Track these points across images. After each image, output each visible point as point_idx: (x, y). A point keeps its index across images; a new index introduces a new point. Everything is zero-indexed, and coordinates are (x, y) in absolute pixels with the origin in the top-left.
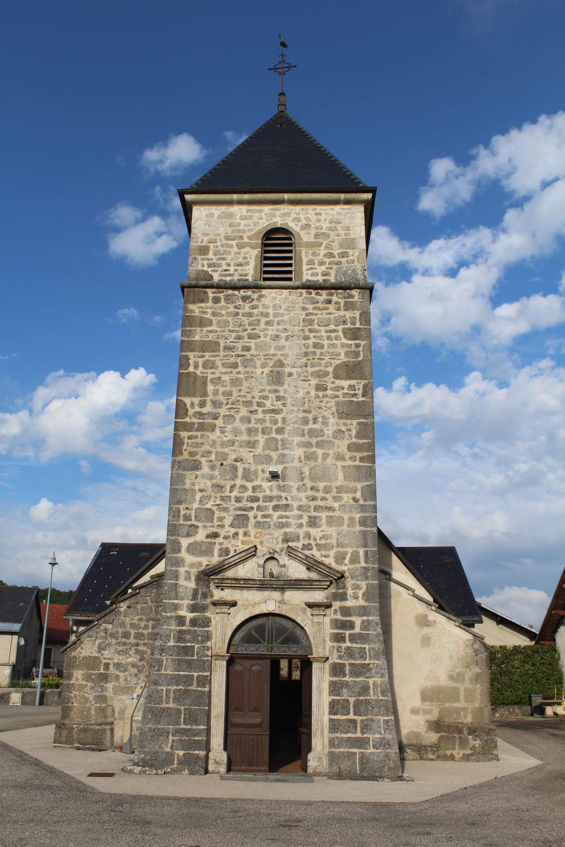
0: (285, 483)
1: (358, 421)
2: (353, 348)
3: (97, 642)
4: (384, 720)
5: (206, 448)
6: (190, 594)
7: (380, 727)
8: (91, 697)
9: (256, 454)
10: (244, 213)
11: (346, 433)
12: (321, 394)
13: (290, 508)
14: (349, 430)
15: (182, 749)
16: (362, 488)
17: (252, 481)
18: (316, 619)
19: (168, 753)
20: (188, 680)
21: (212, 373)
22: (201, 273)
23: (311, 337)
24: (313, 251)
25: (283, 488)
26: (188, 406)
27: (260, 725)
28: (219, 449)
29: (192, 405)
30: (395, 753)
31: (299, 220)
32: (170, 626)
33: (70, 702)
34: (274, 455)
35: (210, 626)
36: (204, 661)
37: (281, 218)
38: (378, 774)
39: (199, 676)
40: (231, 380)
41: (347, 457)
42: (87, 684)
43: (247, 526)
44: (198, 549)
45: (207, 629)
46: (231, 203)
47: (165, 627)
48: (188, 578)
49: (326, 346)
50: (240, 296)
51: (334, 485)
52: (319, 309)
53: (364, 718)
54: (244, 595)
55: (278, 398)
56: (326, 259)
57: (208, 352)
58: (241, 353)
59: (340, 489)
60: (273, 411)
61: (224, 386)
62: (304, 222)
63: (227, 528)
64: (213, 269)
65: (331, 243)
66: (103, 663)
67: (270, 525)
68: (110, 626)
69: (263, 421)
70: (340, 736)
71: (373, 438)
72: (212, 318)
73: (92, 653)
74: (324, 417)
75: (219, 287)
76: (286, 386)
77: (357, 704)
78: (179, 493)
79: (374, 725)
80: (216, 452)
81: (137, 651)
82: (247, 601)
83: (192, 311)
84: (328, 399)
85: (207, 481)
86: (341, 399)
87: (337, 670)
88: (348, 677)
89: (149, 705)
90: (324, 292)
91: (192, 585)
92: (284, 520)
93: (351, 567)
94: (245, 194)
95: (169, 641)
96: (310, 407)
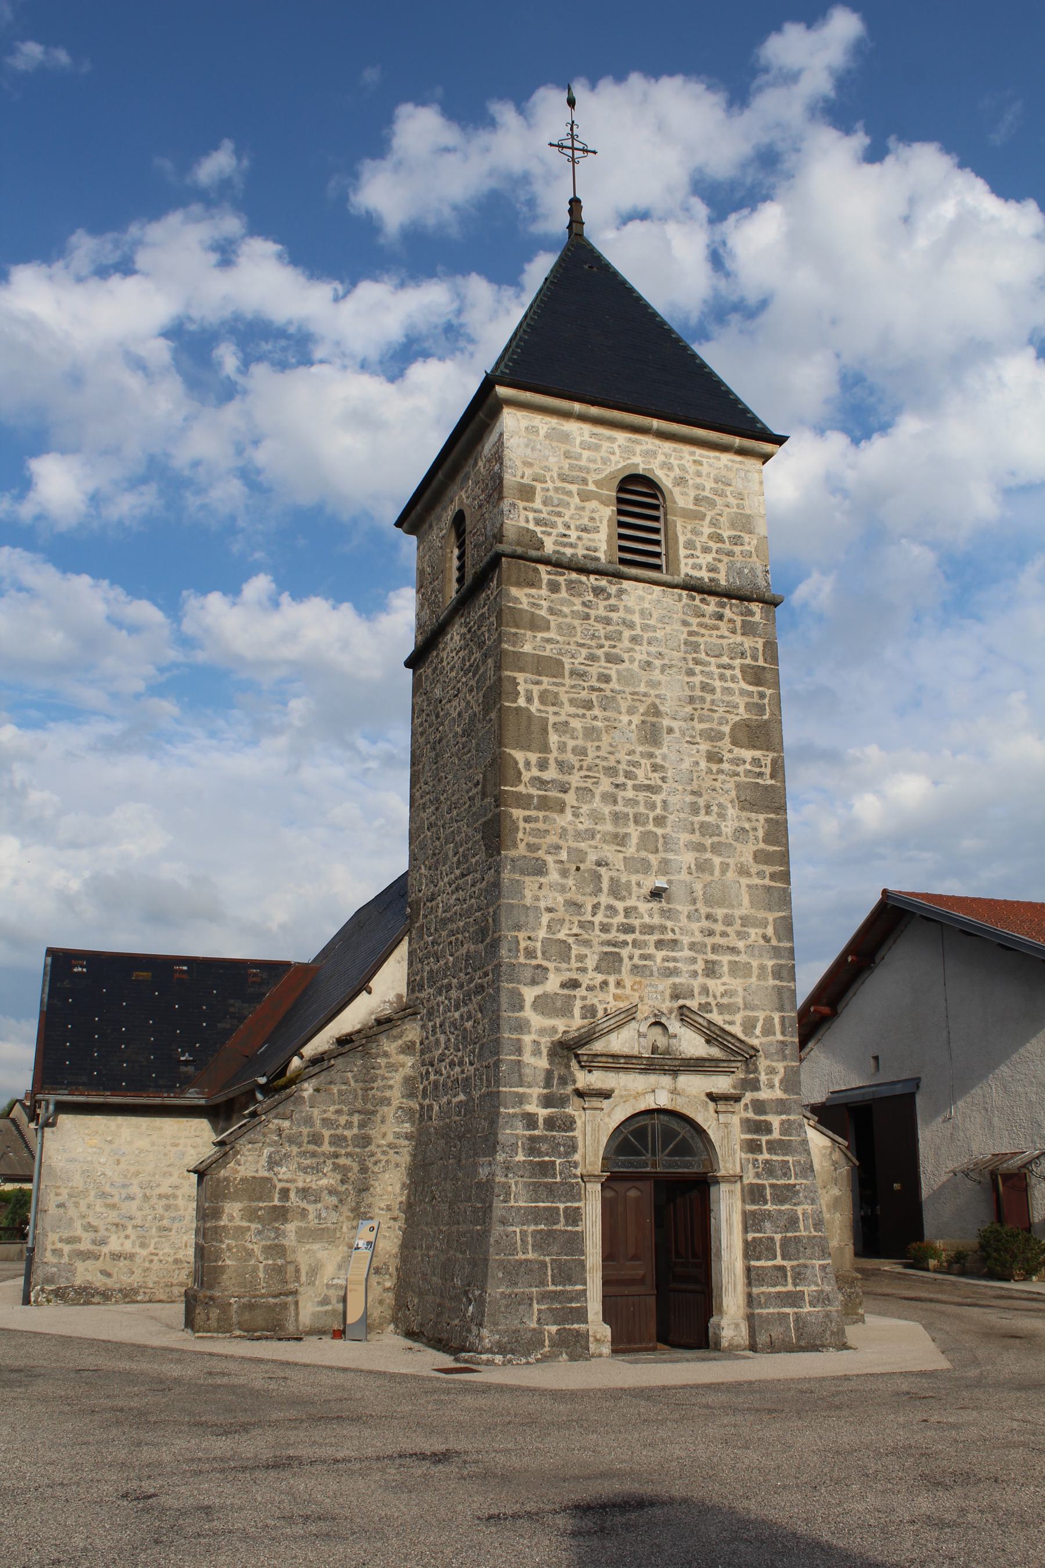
0: (671, 906)
2: (756, 700)
3: (266, 1152)
4: (820, 1265)
5: (552, 839)
6: (541, 1077)
7: (816, 1276)
8: (257, 1249)
9: (627, 855)
10: (586, 438)
11: (751, 833)
12: (714, 767)
13: (679, 945)
14: (755, 829)
15: (555, 1323)
16: (775, 920)
17: (622, 899)
19: (534, 1330)
21: (555, 713)
22: (525, 532)
23: (697, 671)
24: (693, 526)
25: (668, 914)
26: (521, 766)
27: (642, 1281)
28: (572, 844)
29: (528, 764)
30: (837, 1311)
31: (670, 468)
33: (221, 1258)
36: (572, 1185)
37: (643, 459)
38: (818, 1342)
39: (566, 1208)
40: (585, 728)
42: (249, 1227)
43: (620, 972)
45: (571, 1134)
46: (567, 415)
47: (508, 1131)
48: (536, 1052)
49: (718, 690)
50: (590, 585)
51: (737, 913)
53: (795, 1263)
54: (621, 1081)
55: (655, 768)
56: (711, 544)
57: (547, 676)
58: (597, 685)
59: (745, 921)
60: (649, 788)
62: (677, 472)
63: (591, 974)
64: (544, 529)
65: (718, 517)
66: (277, 1189)
67: (652, 971)
68: (286, 1124)
71: (787, 845)
72: (549, 617)
73: (257, 1171)
74: (720, 805)
75: (558, 564)
76: (665, 750)
77: (785, 1242)
78: (515, 912)
80: (569, 848)
82: (626, 1090)
83: (517, 600)
84: (724, 777)
85: (557, 894)
86: (743, 779)
87: (754, 1194)
88: (769, 1204)
89: (497, 1257)
90: (713, 600)
91: (543, 1063)
92: (671, 965)
93: (764, 1040)
94: (593, 406)
95: (517, 1154)
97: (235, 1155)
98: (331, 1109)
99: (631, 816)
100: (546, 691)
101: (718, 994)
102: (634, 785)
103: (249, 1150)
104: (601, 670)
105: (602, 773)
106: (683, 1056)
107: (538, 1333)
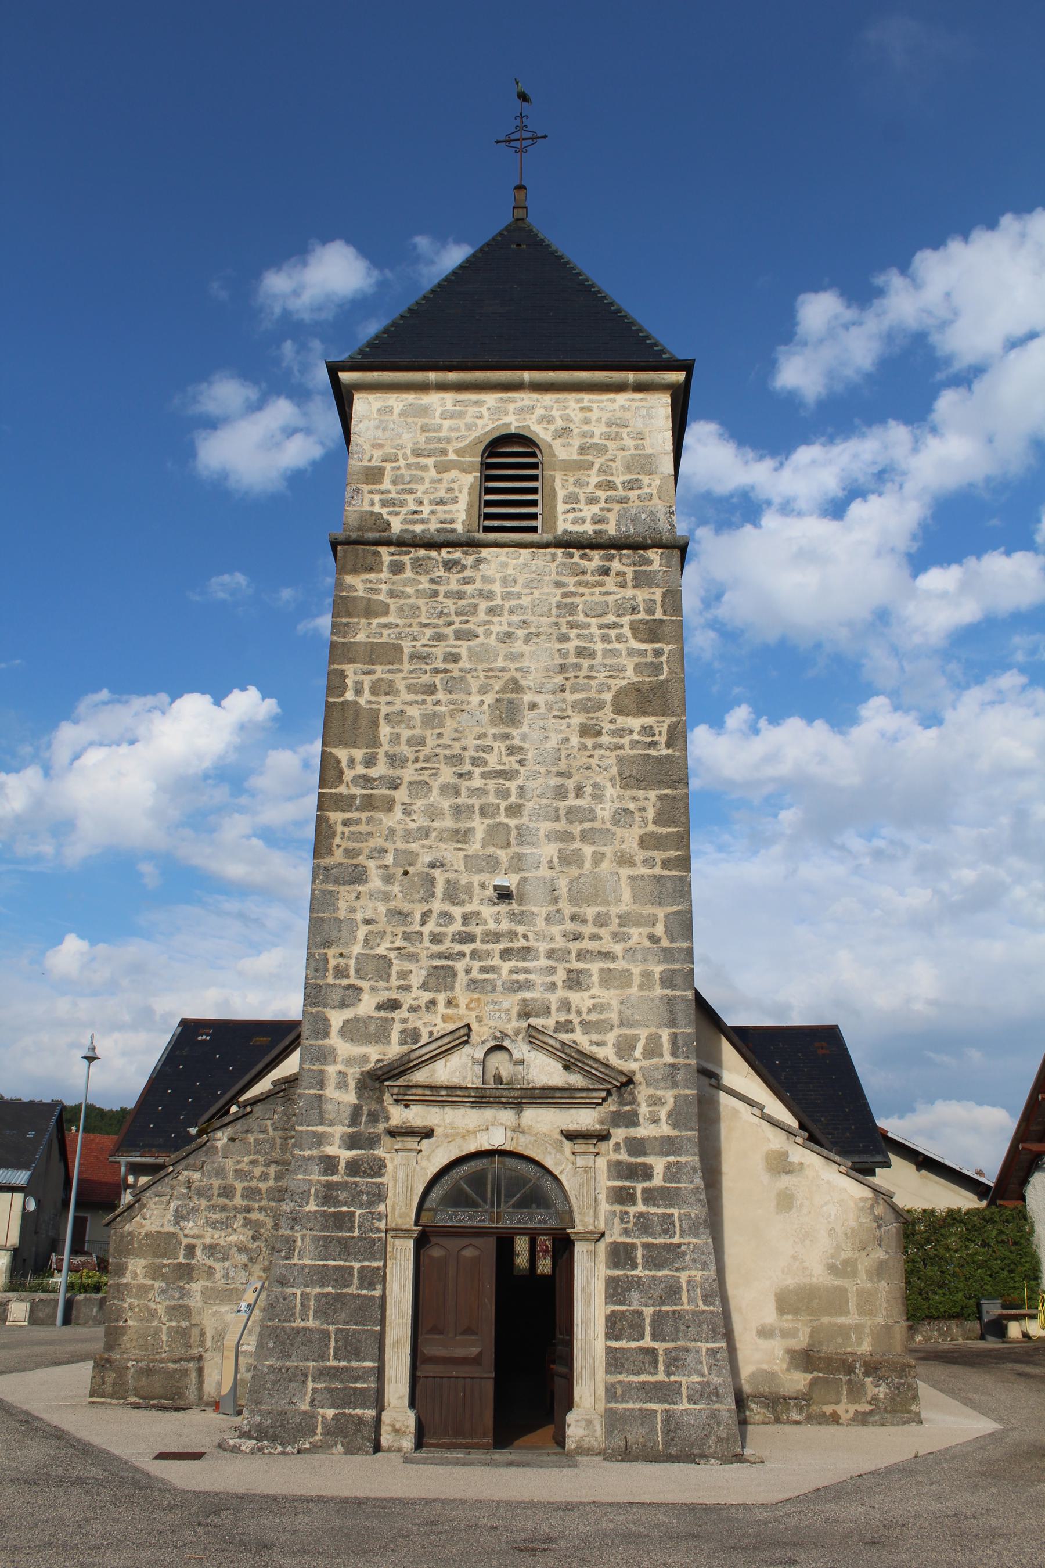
0: (524, 908)
1: (658, 792)
2: (650, 658)
3: (173, 1205)
5: (377, 842)
6: (346, 1114)
7: (701, 1363)
8: (161, 1310)
9: (470, 853)
10: (449, 407)
11: (637, 815)
12: (590, 742)
13: (533, 953)
14: (643, 809)
15: (332, 1406)
16: (667, 917)
17: (462, 903)
18: (580, 1161)
19: (305, 1413)
20: (343, 1276)
21: (389, 703)
23: (572, 636)
24: (576, 477)
26: (344, 764)
27: (476, 1360)
28: (400, 845)
29: (352, 762)
30: (729, 1411)
31: (550, 420)
33: (122, 1318)
34: (503, 855)
38: (696, 1451)
39: (362, 1268)
40: (424, 716)
43: (452, 988)
44: (362, 1030)
45: (378, 1180)
46: (424, 387)
47: (300, 1177)
48: (342, 1085)
49: (599, 653)
50: (440, 560)
51: (614, 910)
52: (587, 584)
53: (670, 1345)
54: (446, 1117)
55: (511, 751)
57: (381, 664)
58: (442, 666)
59: (625, 919)
60: (502, 774)
62: (559, 423)
63: (415, 992)
65: (610, 463)
66: (183, 1245)
68: (196, 1176)
69: (482, 792)
70: (627, 1379)
71: (687, 825)
72: (389, 601)
73: (162, 1226)
74: (595, 785)
75: (403, 543)
76: (525, 728)
77: (658, 1319)
78: (325, 926)
79: (690, 1358)
80: (396, 850)
81: (247, 1223)
82: (453, 1128)
84: (603, 752)
87: (620, 1255)
88: (640, 1268)
89: (270, 1324)
90: (596, 554)
91: (350, 1097)
92: (521, 977)
93: (645, 1063)
94: (450, 371)
95: (307, 1203)
96: (569, 766)
97: (141, 1209)
98: (245, 1159)
99: (477, 808)
100: (380, 680)
101: (584, 1010)
102: (483, 773)
103: (155, 1203)
104: (449, 649)
105: (443, 763)
106: (531, 1085)
107: (309, 1418)
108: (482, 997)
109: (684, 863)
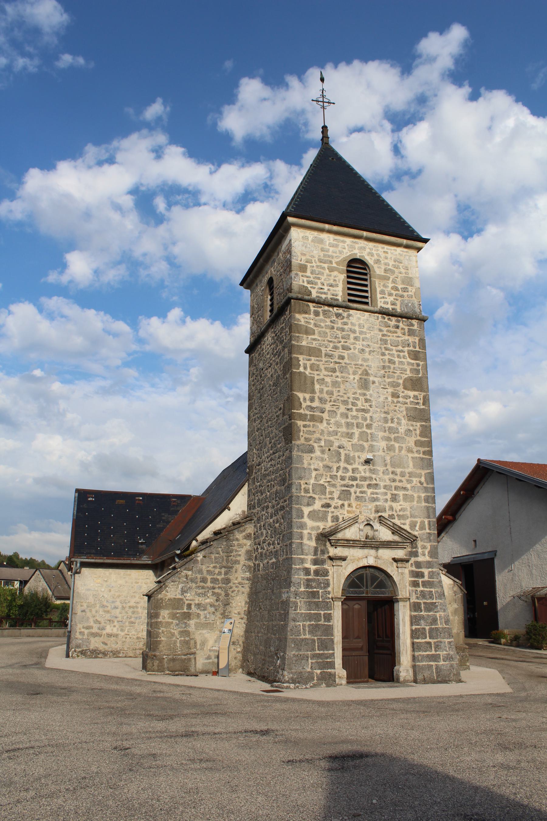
0: (374, 467)
2: (415, 367)
4: (448, 642)
5: (317, 435)
6: (312, 550)
8: (176, 633)
9: (353, 443)
10: (332, 241)
11: (413, 432)
12: (395, 400)
13: (379, 486)
14: (415, 430)
15: (319, 669)
16: (425, 474)
17: (351, 464)
18: (400, 570)
19: (309, 672)
20: (317, 617)
21: (318, 375)
22: (302, 287)
23: (386, 353)
24: (384, 283)
26: (302, 400)
27: (361, 649)
29: (305, 399)
30: (456, 664)
32: (300, 576)
33: (159, 637)
34: (365, 444)
35: (328, 576)
38: (447, 679)
39: (325, 614)
40: (332, 382)
41: (415, 450)
43: (350, 499)
44: (316, 515)
45: (327, 578)
46: (322, 230)
47: (296, 577)
48: (310, 539)
49: (397, 362)
50: (334, 312)
51: (407, 471)
52: (391, 332)
53: (436, 640)
54: (351, 552)
55: (367, 401)
56: (393, 292)
58: (338, 361)
59: (411, 474)
60: (363, 410)
61: (327, 387)
63: (336, 500)
65: (396, 279)
67: (365, 499)
68: (190, 573)
69: (356, 417)
70: (422, 654)
73: (176, 595)
74: (398, 418)
75: (318, 302)
76: (371, 392)
77: (431, 630)
78: (299, 471)
79: (442, 645)
81: (214, 593)
82: (353, 557)
83: (299, 320)
84: (400, 405)
86: (409, 405)
87: (416, 607)
88: (423, 612)
90: (394, 319)
91: (313, 544)
92: (375, 496)
93: (420, 532)
95: (300, 587)
96: (388, 409)
98: (211, 565)
99: (355, 424)
101: (398, 510)
102: (356, 409)
103: (172, 585)
104: (340, 353)
108: (361, 503)
109: (430, 453)
